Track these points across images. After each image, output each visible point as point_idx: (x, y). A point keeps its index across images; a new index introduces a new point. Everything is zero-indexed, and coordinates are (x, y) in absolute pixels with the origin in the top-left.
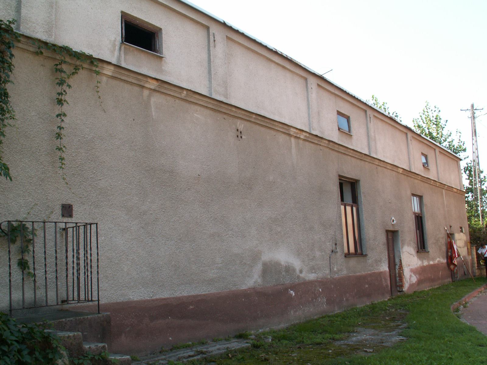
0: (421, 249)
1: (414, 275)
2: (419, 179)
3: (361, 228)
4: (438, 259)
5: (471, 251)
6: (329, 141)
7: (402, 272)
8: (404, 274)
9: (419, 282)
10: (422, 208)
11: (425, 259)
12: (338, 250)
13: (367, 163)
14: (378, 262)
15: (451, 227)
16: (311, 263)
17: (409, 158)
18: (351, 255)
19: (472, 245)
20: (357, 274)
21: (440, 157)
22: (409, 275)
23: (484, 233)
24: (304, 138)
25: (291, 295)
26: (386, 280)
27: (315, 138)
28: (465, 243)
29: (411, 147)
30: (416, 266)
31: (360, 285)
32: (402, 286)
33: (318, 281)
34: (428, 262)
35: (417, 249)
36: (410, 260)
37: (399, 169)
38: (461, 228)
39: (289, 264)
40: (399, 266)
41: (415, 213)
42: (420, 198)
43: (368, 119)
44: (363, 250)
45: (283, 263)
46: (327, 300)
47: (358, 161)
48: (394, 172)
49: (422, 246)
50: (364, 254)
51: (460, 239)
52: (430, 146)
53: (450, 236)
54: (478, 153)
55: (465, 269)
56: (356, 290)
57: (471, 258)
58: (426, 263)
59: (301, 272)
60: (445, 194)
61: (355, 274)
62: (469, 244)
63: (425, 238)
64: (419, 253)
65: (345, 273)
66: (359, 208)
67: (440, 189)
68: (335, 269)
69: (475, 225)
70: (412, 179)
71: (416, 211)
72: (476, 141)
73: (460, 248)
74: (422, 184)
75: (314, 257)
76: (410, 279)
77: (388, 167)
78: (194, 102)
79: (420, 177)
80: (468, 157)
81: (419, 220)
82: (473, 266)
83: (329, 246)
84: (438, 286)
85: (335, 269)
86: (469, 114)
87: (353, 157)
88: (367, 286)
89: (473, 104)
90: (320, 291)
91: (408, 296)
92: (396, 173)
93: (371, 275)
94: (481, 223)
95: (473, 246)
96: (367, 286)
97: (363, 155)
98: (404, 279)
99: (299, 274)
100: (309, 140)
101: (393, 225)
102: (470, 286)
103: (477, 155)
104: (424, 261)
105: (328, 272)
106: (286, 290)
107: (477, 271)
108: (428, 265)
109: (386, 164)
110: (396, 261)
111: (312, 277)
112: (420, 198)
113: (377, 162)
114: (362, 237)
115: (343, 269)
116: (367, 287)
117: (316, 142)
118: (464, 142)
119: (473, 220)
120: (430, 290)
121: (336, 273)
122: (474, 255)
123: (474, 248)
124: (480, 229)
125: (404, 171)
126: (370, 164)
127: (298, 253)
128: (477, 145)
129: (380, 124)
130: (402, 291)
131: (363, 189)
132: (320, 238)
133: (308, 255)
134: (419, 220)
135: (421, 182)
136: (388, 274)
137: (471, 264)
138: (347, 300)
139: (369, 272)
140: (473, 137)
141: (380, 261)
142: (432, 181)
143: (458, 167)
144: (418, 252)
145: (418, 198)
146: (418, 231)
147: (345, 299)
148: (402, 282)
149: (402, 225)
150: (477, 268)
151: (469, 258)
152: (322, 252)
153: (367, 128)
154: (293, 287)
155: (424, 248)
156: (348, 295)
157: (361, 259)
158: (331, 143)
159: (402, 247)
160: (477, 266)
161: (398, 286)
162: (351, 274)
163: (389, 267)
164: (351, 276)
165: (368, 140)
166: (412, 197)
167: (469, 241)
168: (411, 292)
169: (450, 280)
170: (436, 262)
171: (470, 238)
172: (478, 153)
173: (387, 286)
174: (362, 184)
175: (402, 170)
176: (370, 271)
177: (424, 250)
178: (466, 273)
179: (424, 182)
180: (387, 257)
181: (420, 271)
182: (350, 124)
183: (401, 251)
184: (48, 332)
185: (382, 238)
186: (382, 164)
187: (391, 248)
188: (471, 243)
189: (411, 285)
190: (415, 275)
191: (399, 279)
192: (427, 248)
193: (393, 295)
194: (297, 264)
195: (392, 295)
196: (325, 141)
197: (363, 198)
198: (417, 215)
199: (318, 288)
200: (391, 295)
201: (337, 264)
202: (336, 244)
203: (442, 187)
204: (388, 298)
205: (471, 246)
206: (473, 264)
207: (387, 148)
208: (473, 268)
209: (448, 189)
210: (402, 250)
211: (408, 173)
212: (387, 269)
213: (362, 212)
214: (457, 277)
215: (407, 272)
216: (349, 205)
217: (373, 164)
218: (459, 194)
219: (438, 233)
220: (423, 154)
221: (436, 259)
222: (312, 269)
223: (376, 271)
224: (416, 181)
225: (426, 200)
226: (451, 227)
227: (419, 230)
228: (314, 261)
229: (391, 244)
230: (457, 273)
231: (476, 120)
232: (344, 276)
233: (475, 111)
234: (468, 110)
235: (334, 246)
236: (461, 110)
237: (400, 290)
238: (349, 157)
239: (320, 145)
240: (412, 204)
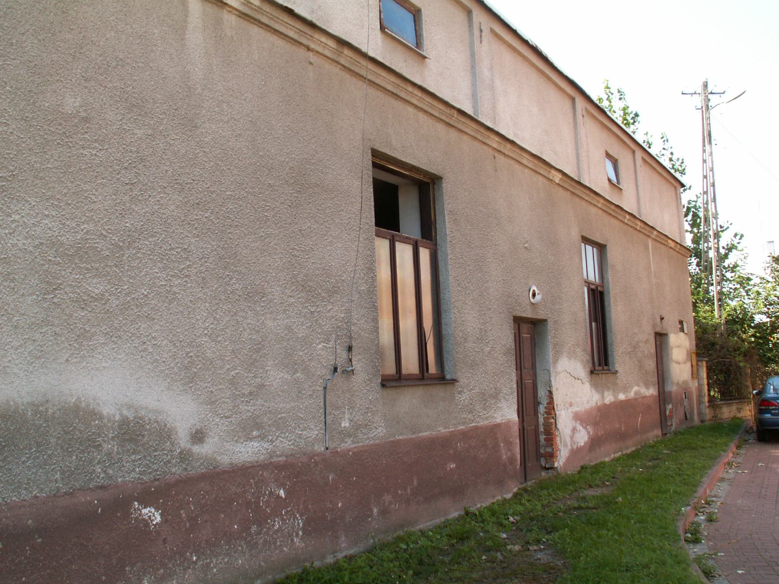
0: (600, 365)
1: (581, 428)
2: (599, 205)
3: (443, 307)
4: (636, 388)
5: (698, 370)
6: (343, 43)
7: (553, 420)
8: (559, 426)
9: (594, 443)
10: (604, 273)
11: (608, 389)
12: (357, 365)
13: (465, 137)
14: (491, 397)
15: (662, 319)
16: (243, 407)
17: (578, 155)
18: (407, 379)
19: (699, 358)
21: (644, 172)
22: (571, 428)
23: (722, 334)
24: (241, 8)
25: (146, 523)
26: (509, 444)
27: (286, 18)
28: (687, 354)
29: (582, 131)
30: (587, 406)
31: (423, 465)
32: (551, 456)
33: (271, 463)
34: (614, 396)
35: (590, 365)
36: (573, 392)
37: (553, 171)
38: (681, 322)
39: (143, 413)
40: (545, 408)
41: (588, 283)
42: (601, 248)
43: (476, 33)
44: (447, 368)
45: (106, 411)
46: (307, 523)
47: (440, 127)
48: (540, 178)
49: (601, 360)
50: (448, 377)
51: (679, 347)
52: (624, 143)
53: (661, 337)
54: (713, 177)
55: (687, 407)
56: (415, 483)
57: (697, 385)
58: (609, 398)
59: (198, 437)
60: (652, 248)
62: (694, 356)
63: (609, 341)
64: (593, 375)
65: (379, 432)
66: (440, 253)
67: (641, 236)
68: (345, 424)
69: (705, 318)
70: (584, 203)
71: (591, 278)
72: (711, 154)
73: (679, 363)
74: (606, 218)
75: (261, 386)
76: (571, 435)
77: (525, 162)
79: (602, 201)
80: (690, 189)
81: (598, 298)
82: (700, 402)
83: (324, 353)
84: (634, 449)
85: (345, 424)
86: (698, 101)
87: (426, 112)
88: (453, 466)
89: (707, 82)
90: (279, 497)
91: (565, 482)
92: (545, 181)
94: (717, 316)
95: (702, 361)
96: (453, 466)
97: (455, 112)
98: (558, 439)
99: (189, 446)
100: (264, 20)
101: (533, 304)
102: (703, 448)
103: (712, 181)
104: (606, 393)
105: (314, 432)
107: (707, 411)
108: (614, 402)
109: (518, 151)
110: (540, 395)
111: (248, 451)
112: (601, 248)
113: (494, 141)
114: (444, 332)
115: (371, 420)
116: (451, 470)
118: (683, 160)
119: (704, 308)
120: (618, 459)
121: (345, 434)
122: (703, 378)
123: (704, 363)
124: (716, 327)
125: (565, 178)
126: (476, 143)
127: (189, 374)
128: (712, 162)
129: (507, 57)
130: (552, 468)
131: (452, 202)
132: (289, 328)
133: (233, 382)
134: (598, 298)
135: (604, 214)
136: (516, 429)
137: (697, 396)
138: (384, 512)
139: (462, 427)
140: (704, 146)
141: (496, 396)
142: (628, 217)
143: (677, 200)
144: (592, 372)
145: (595, 249)
146: (593, 323)
147: (375, 510)
148: (552, 445)
149: (557, 307)
150: (707, 404)
151: (693, 385)
152: (296, 371)
153: (473, 55)
155: (606, 364)
156: (387, 498)
157: (438, 391)
158: (347, 52)
159: (556, 361)
160: (709, 402)
161: (542, 456)
162: (401, 434)
163: (521, 412)
164: (401, 440)
165: (474, 85)
166: (583, 245)
167: (695, 351)
168: (572, 470)
169: (658, 432)
170: (632, 394)
171: (697, 345)
172: (713, 177)
173: (512, 460)
174: (447, 187)
175: (560, 176)
177: (605, 368)
178: (688, 417)
179: (610, 214)
180: (515, 386)
181: (597, 419)
182: (421, 29)
183: (551, 369)
185: (503, 337)
186: (507, 148)
187: (527, 364)
188: (698, 355)
189: (575, 453)
190: (585, 428)
191: (545, 440)
192: (614, 363)
193: (528, 478)
194: (178, 411)
195: (526, 480)
196: (324, 39)
197: (449, 227)
198: (593, 287)
199: (273, 487)
200: (523, 480)
201: (352, 408)
202: (350, 349)
203: (646, 232)
204: (515, 490)
205: (697, 361)
206: (700, 396)
207: (519, 112)
208: (700, 404)
209: (658, 239)
210: (554, 366)
211: (575, 186)
212: (514, 417)
213: (446, 264)
214: (672, 425)
215: (565, 422)
216: (406, 240)
217: (485, 143)
218: (678, 252)
219: (636, 331)
220: (608, 156)
221: (632, 389)
222: (252, 427)
223: (482, 423)
224: (593, 210)
225: (614, 255)
226: (662, 319)
227: (596, 321)
229: (527, 352)
230: (671, 417)
231: (712, 112)
232: (377, 442)
233: (710, 96)
234: (695, 93)
235: (344, 355)
236: (683, 94)
237: (547, 466)
238: (411, 109)
239: (308, 49)
240: (581, 259)
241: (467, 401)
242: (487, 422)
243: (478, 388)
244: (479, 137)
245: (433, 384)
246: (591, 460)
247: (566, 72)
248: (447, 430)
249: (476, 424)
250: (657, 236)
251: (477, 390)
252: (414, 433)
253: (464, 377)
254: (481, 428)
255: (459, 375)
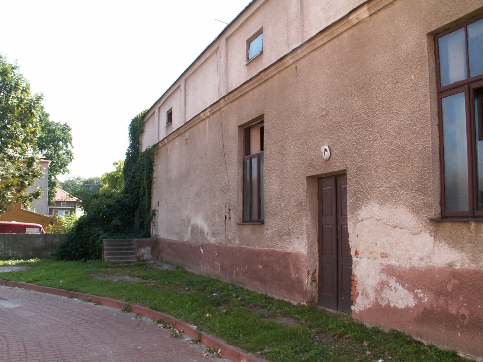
12: (232, 216)
20: (250, 247)
37: (351, 17)
61: (247, 247)
68: (230, 237)
78: (239, 97)
83: (224, 211)
88: (261, 267)
91: (362, 333)
93: (268, 253)
96: (261, 267)
106: (198, 248)
111: (212, 240)
117: (218, 108)
127: (206, 219)
139: (266, 248)
154: (203, 246)
159: (356, 208)
162: (244, 245)
176: (268, 247)
184: (112, 262)
202: (229, 210)
222: (214, 234)
228: (215, 227)
241: (269, 235)
242: (281, 249)
243: (276, 228)
244: (280, 69)
245: (448, 221)
246: (410, 329)
247: (216, 36)
248: (259, 248)
249: (274, 249)
250: (164, 142)
251: (275, 229)
252: (248, 246)
253: (269, 221)
254: (276, 252)
255: (266, 220)
